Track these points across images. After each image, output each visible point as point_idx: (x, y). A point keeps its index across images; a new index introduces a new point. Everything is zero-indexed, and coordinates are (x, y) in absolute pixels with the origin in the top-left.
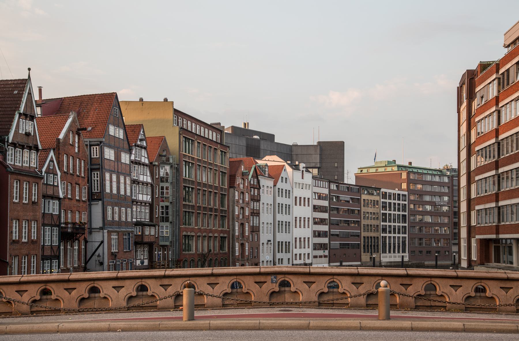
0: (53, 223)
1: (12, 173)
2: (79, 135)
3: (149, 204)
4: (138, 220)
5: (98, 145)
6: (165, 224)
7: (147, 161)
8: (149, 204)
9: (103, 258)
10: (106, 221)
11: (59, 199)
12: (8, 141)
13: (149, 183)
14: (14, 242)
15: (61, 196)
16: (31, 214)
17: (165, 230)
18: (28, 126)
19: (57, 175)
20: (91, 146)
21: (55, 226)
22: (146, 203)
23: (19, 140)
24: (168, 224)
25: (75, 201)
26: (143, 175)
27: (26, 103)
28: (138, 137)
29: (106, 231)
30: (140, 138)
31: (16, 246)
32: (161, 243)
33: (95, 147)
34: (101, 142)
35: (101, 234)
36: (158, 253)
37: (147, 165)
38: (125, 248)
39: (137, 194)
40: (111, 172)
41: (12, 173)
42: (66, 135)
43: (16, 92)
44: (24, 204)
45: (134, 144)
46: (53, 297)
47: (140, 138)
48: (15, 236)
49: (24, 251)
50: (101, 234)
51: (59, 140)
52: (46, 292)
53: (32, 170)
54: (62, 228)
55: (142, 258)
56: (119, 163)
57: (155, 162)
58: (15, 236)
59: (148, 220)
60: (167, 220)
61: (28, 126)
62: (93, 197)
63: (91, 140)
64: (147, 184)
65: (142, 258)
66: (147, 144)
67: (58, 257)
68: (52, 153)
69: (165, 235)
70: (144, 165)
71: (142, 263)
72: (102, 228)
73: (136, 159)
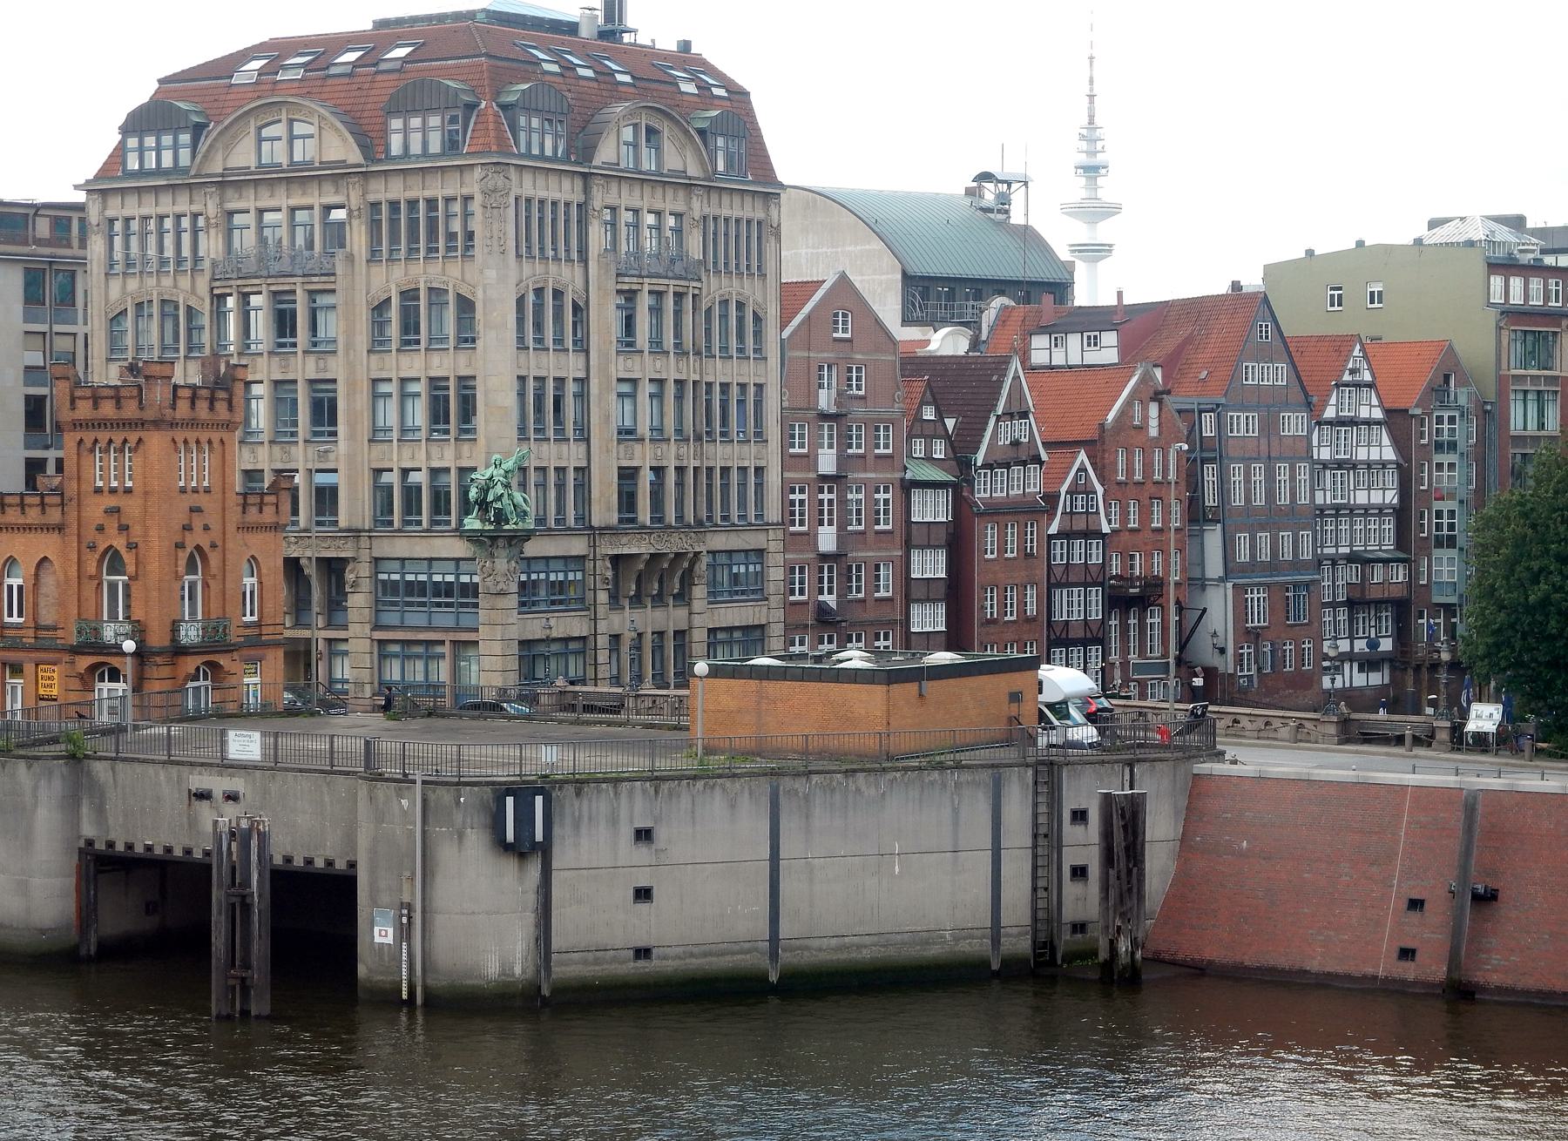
0: (1089, 579)
1: (981, 514)
2: (1160, 402)
3: (1394, 509)
4: (1354, 549)
5: (1212, 411)
6: (1445, 554)
7: (1378, 414)
8: (1394, 509)
9: (1226, 639)
10: (1230, 565)
11: (1103, 536)
12: (975, 464)
13: (1390, 462)
14: (992, 622)
15: (1106, 529)
16: (1023, 573)
17: (1445, 569)
18: (1018, 430)
19: (1096, 493)
20: (1200, 412)
21: (1094, 584)
22: (1381, 510)
23: (999, 457)
24: (1454, 553)
25: (1150, 532)
26: (1369, 446)
27: (1009, 394)
28: (1345, 366)
29: (1229, 585)
30: (1350, 366)
31: (992, 629)
32: (1437, 599)
33: (1208, 415)
34: (1218, 405)
35: (1222, 591)
36: (1428, 621)
37: (1378, 423)
38: (1291, 614)
39: (1349, 490)
40: (1247, 461)
41: (981, 514)
42: (1123, 412)
43: (995, 378)
44: (1007, 559)
45: (1333, 383)
46: (1241, 725)
47: (1350, 366)
48: (991, 610)
49: (1009, 636)
50: (1222, 591)
51: (1102, 425)
52: (1236, 721)
53: (1029, 499)
54: (1112, 587)
55: (1373, 636)
56: (1273, 438)
57: (1417, 406)
58: (991, 610)
59: (1392, 547)
60: (1451, 542)
61: (1018, 430)
62: (1197, 514)
63: (1202, 400)
64: (1384, 465)
65: (1373, 636)
66: (1373, 375)
67: (1101, 641)
68: (1082, 456)
69: (1445, 578)
70: (1369, 423)
71: (1373, 644)
72: (1223, 580)
73: (1340, 414)
